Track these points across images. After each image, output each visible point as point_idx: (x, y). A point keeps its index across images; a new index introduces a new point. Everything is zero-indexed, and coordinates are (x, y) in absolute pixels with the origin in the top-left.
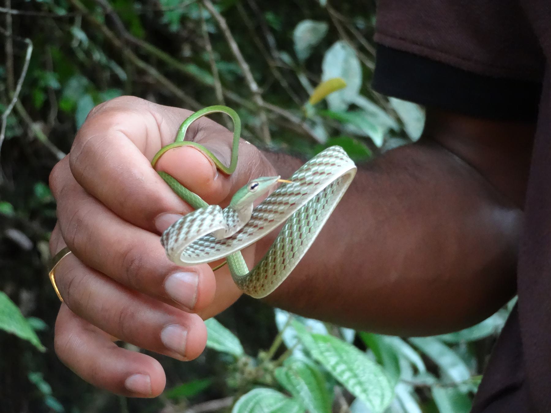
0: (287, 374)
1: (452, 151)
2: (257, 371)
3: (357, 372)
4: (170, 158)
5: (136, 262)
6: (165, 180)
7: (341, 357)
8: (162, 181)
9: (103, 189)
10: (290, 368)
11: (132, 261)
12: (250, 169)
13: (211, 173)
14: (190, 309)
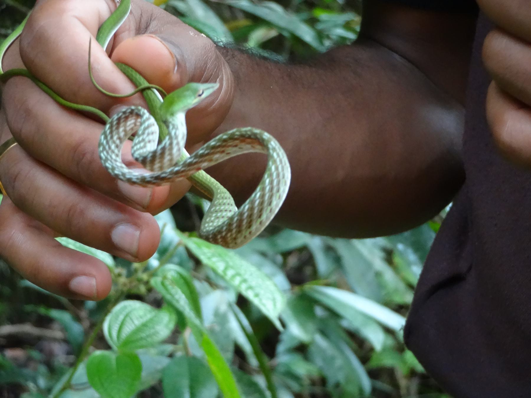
0: (163, 284)
1: (392, 49)
2: (131, 282)
3: (246, 277)
4: (131, 44)
5: (88, 156)
6: (121, 70)
7: (227, 263)
8: (120, 71)
9: (56, 77)
10: (165, 278)
11: (84, 155)
12: (206, 63)
13: (171, 65)
14: (143, 208)
